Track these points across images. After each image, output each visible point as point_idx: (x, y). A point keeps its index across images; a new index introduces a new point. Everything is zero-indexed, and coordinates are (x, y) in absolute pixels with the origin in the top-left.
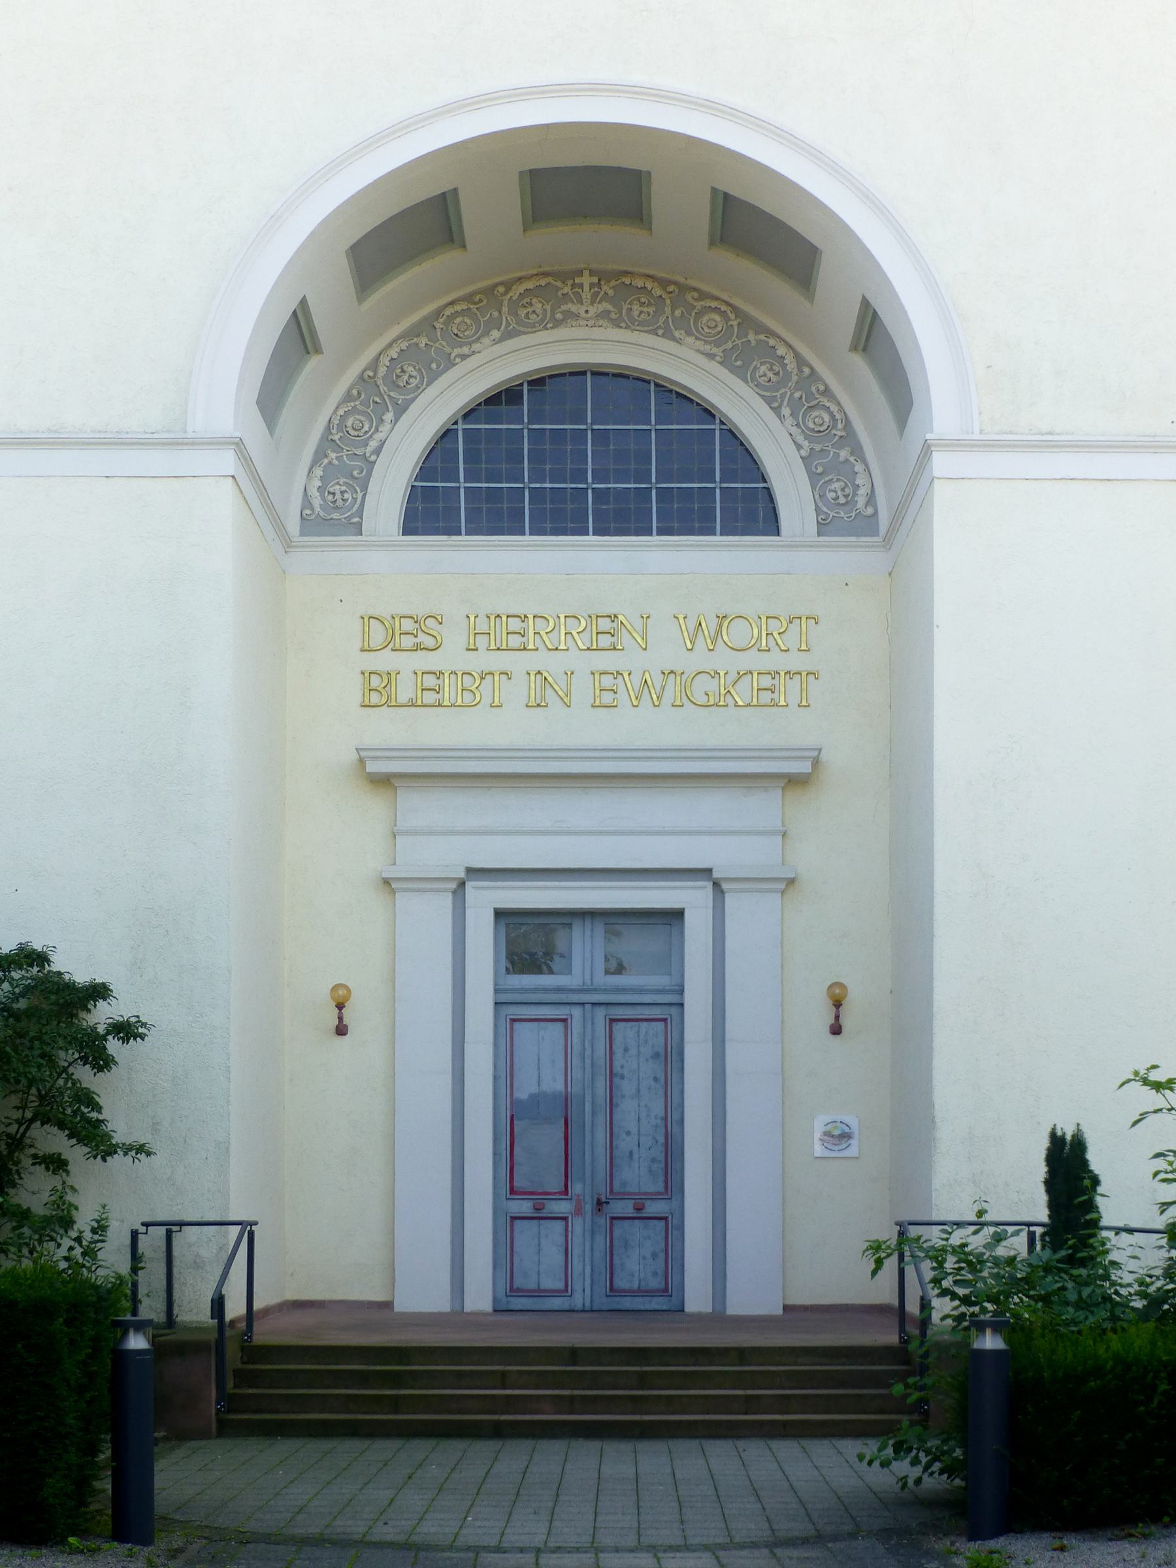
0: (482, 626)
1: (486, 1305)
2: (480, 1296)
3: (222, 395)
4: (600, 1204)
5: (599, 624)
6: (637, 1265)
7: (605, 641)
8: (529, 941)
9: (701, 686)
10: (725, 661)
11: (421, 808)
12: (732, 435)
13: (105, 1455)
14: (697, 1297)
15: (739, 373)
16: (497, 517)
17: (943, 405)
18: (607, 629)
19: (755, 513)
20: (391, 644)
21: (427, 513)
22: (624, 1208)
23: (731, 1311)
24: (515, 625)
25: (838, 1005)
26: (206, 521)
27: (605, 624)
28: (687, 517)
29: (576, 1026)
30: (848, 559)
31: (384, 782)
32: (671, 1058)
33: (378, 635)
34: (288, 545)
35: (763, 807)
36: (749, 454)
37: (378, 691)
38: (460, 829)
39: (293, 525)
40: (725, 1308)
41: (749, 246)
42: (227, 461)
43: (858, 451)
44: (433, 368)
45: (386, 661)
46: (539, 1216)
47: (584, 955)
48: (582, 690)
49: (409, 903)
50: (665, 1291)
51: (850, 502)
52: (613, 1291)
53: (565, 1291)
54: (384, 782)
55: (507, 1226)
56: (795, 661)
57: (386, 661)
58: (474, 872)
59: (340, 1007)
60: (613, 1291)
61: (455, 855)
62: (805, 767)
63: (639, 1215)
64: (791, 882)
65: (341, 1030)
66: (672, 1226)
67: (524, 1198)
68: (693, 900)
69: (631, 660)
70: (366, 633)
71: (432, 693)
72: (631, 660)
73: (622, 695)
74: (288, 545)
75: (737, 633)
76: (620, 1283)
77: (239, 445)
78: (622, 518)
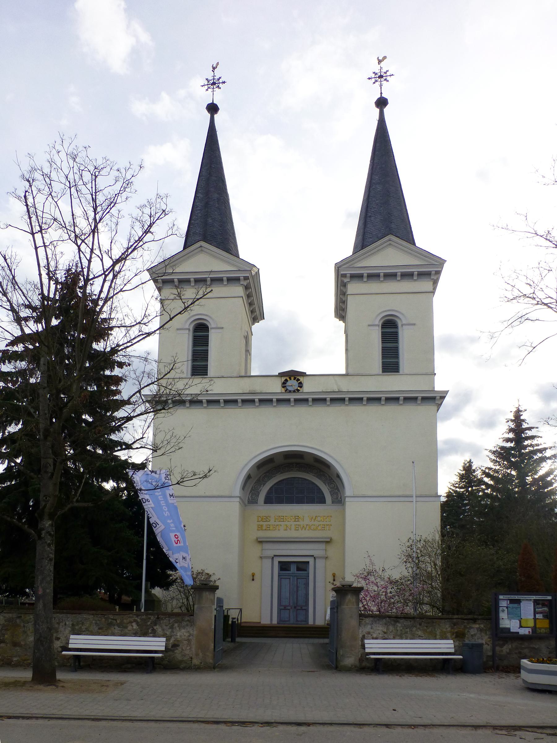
0: (277, 518)
1: (276, 623)
2: (275, 622)
3: (237, 491)
4: (295, 607)
5: (296, 521)
6: (301, 617)
7: (297, 520)
8: (284, 566)
9: (312, 527)
10: (316, 523)
11: (266, 546)
12: (317, 486)
13: (122, 422)
14: (311, 622)
15: (320, 479)
16: (280, 501)
17: (348, 491)
18: (297, 518)
19: (322, 500)
20: (262, 520)
21: (268, 500)
22: (299, 608)
23: (436, 390)
24: (282, 517)
25: (334, 576)
26: (235, 506)
27: (297, 517)
28: (311, 501)
29: (291, 579)
30: (336, 507)
31: (261, 542)
32: (307, 585)
33: (260, 519)
34: (246, 506)
35: (322, 546)
36: (320, 489)
37: (260, 528)
38: (271, 550)
39: (246, 502)
40: (434, 388)
41: (318, 466)
42: (238, 499)
43: (339, 490)
44: (270, 478)
45: (261, 523)
46: (285, 609)
47: (293, 568)
48: (293, 527)
49: (265, 560)
50: (305, 621)
51: (337, 498)
52: (297, 621)
53: (289, 621)
54: (261, 542)
55: (279, 611)
56: (328, 523)
57: (261, 523)
58: (275, 556)
59: (253, 576)
60: (297, 621)
61: (271, 553)
62: (329, 540)
63: (302, 609)
64: (327, 557)
65: (253, 580)
66: (307, 611)
67: (282, 608)
68: (311, 560)
69: (301, 523)
70: (258, 519)
71: (268, 528)
72: (301, 523)
73: (300, 529)
74: (246, 506)
75: (319, 519)
76: (299, 619)
77: (240, 497)
78: (300, 501)
